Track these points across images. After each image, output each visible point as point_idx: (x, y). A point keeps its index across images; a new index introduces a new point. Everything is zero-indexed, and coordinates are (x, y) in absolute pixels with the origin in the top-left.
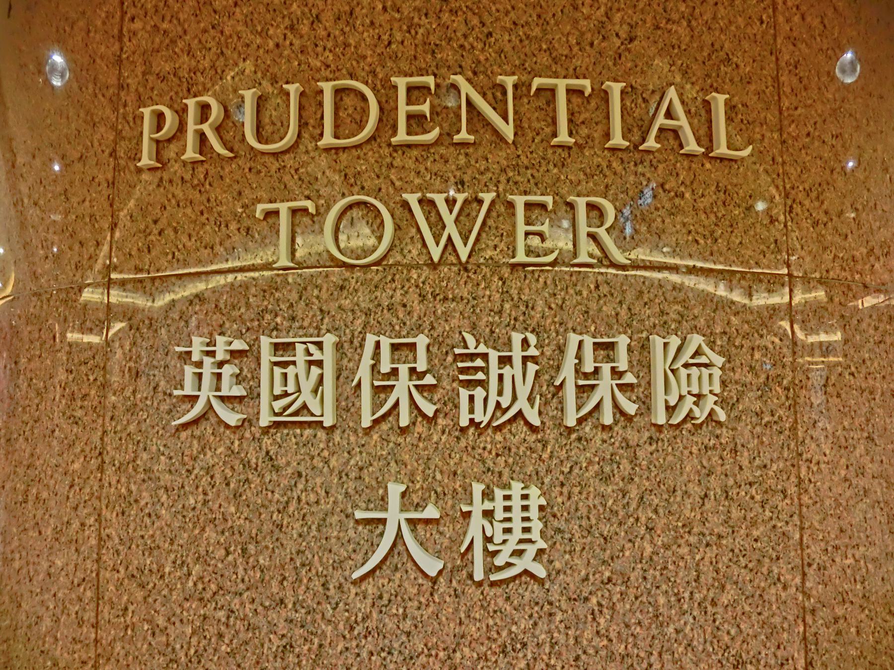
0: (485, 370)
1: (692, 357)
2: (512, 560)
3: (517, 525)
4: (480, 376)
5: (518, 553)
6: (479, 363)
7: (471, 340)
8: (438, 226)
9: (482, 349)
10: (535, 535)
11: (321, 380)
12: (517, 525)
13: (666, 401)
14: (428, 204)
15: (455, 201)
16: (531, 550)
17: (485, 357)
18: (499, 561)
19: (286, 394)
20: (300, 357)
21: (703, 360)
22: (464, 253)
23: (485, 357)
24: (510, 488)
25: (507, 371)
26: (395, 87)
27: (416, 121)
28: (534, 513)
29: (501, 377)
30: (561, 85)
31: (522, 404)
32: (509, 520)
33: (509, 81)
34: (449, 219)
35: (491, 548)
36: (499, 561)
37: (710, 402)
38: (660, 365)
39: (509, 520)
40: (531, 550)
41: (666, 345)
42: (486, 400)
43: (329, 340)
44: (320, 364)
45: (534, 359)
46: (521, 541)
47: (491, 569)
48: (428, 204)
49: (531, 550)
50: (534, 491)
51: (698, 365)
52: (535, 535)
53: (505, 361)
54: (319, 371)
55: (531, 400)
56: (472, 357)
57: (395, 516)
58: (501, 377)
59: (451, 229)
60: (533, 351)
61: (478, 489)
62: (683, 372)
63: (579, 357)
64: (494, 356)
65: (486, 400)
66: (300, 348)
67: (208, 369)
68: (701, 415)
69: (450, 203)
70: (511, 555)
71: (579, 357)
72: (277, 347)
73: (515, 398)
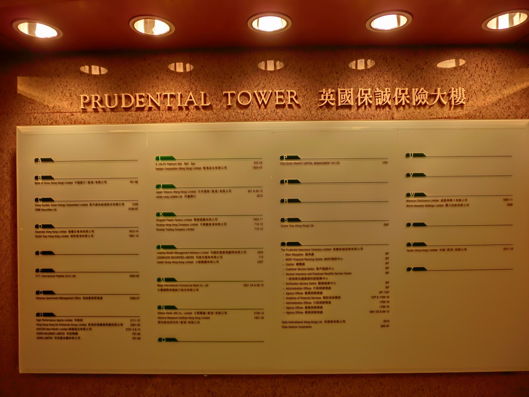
0: (380, 95)
1: (421, 92)
2: (459, 101)
3: (460, 95)
4: (380, 96)
5: (460, 100)
6: (380, 94)
7: (378, 89)
9: (380, 91)
10: (463, 97)
11: (350, 97)
12: (460, 95)
13: (415, 101)
14: (259, 94)
16: (463, 99)
17: (380, 93)
18: (457, 101)
19: (343, 100)
20: (346, 93)
21: (423, 92)
23: (380, 93)
24: (458, 88)
25: (385, 95)
26: (105, 96)
28: (463, 93)
29: (384, 96)
31: (388, 101)
32: (461, 94)
34: (263, 96)
35: (455, 99)
36: (457, 101)
37: (425, 101)
38: (414, 94)
41: (415, 90)
42: (381, 100)
43: (352, 89)
44: (350, 94)
45: (390, 93)
46: (461, 98)
49: (463, 99)
51: (423, 94)
52: (463, 97)
53: (384, 93)
54: (350, 95)
55: (389, 100)
56: (378, 93)
57: (439, 94)
58: (384, 96)
59: (263, 98)
60: (389, 91)
61: (453, 89)
62: (419, 95)
63: (398, 92)
64: (382, 92)
65: (381, 100)
66: (346, 91)
67: (327, 96)
68: (423, 103)
69: (263, 93)
71: (398, 92)
72: (341, 91)
73: (386, 100)
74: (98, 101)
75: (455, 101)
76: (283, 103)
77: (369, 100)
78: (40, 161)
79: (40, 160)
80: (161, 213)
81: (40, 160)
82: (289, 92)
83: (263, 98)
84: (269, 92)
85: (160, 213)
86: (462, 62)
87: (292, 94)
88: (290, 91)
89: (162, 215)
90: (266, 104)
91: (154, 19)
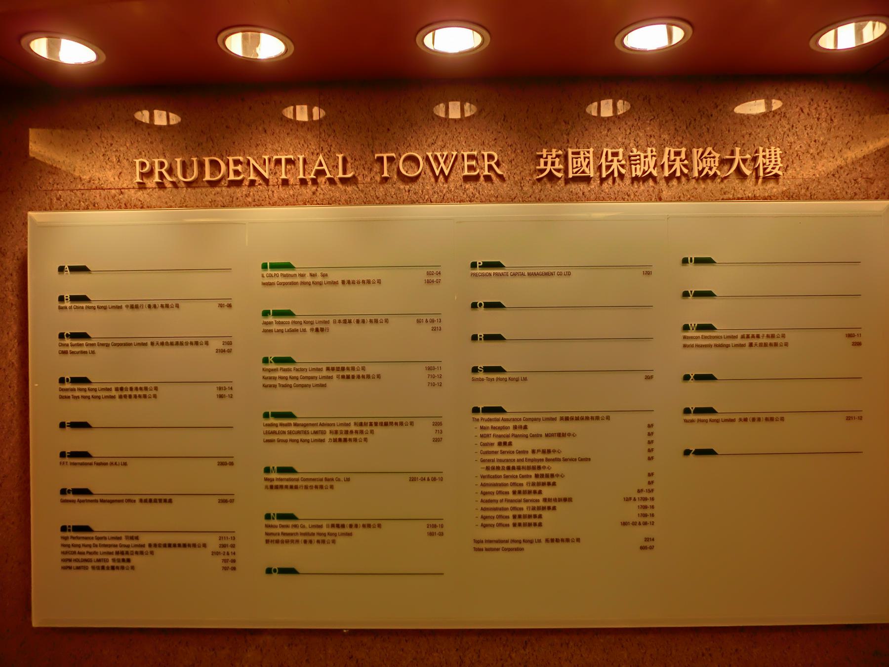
0: (639, 159)
1: (708, 155)
2: (772, 170)
3: (773, 160)
4: (638, 162)
5: (773, 168)
6: (638, 157)
7: (635, 150)
9: (639, 153)
10: (779, 162)
11: (589, 163)
12: (773, 160)
13: (698, 169)
14: (436, 158)
16: (778, 167)
17: (639, 155)
18: (768, 171)
19: (577, 167)
20: (582, 156)
21: (712, 155)
23: (639, 155)
24: (771, 149)
25: (647, 160)
28: (778, 156)
29: (645, 162)
31: (651, 169)
32: (775, 158)
33: (266, 157)
34: (442, 161)
35: (765, 166)
36: (768, 171)
37: (714, 170)
38: (695, 158)
41: (698, 152)
42: (640, 168)
43: (591, 150)
44: (588, 158)
45: (655, 156)
46: (774, 165)
49: (778, 167)
51: (710, 158)
52: (779, 162)
53: (646, 157)
54: (588, 160)
55: (654, 168)
56: (635, 156)
57: (738, 157)
58: (645, 162)
59: (442, 164)
60: (654, 153)
61: (761, 149)
62: (704, 160)
63: (669, 154)
64: (642, 155)
65: (640, 168)
66: (582, 153)
67: (549, 161)
68: (711, 173)
69: (442, 156)
71: (669, 154)
72: (573, 153)
73: (649, 167)
74: (165, 170)
75: (765, 169)
76: (476, 173)
77: (621, 169)
78: (67, 271)
79: (68, 270)
80: (271, 357)
81: (68, 268)
82: (486, 154)
83: (442, 164)
84: (452, 155)
85: (269, 358)
86: (776, 104)
87: (491, 157)
88: (488, 152)
89: (272, 361)
90: (447, 174)
91: (259, 32)
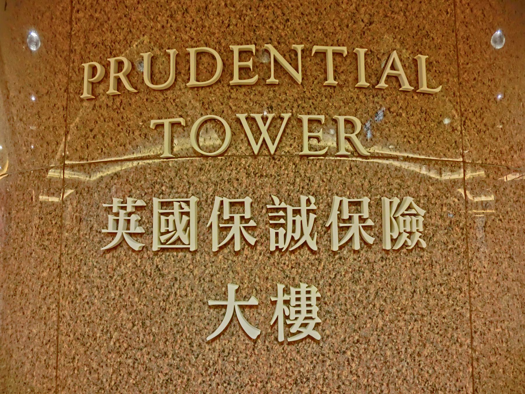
0: (285, 218)
1: (407, 210)
2: (301, 329)
3: (304, 309)
4: (282, 221)
5: (304, 325)
6: (281, 213)
7: (276, 200)
8: (257, 133)
9: (283, 205)
10: (314, 315)
11: (188, 224)
12: (304, 309)
13: (391, 236)
14: (251, 120)
15: (267, 118)
16: (312, 324)
17: (285, 210)
18: (293, 330)
19: (168, 232)
20: (176, 210)
21: (413, 212)
22: (272, 149)
23: (285, 210)
24: (299, 287)
25: (298, 218)
26: (232, 51)
27: (244, 71)
28: (313, 302)
29: (294, 222)
30: (330, 50)
31: (307, 237)
32: (299, 306)
33: (299, 48)
34: (264, 129)
35: (289, 322)
36: (293, 330)
37: (417, 236)
38: (387, 215)
39: (299, 306)
40: (312, 324)
41: (391, 203)
42: (285, 235)
43: (193, 200)
44: (188, 214)
45: (314, 211)
46: (306, 318)
47: (288, 334)
48: (251, 120)
49: (312, 323)
50: (314, 289)
51: (410, 215)
52: (314, 315)
53: (297, 212)
54: (187, 218)
55: (312, 235)
56: (277, 210)
57: (232, 303)
58: (294, 222)
59: (265, 135)
60: (313, 207)
61: (281, 287)
62: (401, 219)
63: (340, 210)
64: (290, 209)
65: (285, 235)
66: (176, 205)
67: (122, 217)
68: (411, 244)
69: (264, 119)
70: (300, 326)
71: (340, 210)
72: (162, 204)
73: (302, 234)
